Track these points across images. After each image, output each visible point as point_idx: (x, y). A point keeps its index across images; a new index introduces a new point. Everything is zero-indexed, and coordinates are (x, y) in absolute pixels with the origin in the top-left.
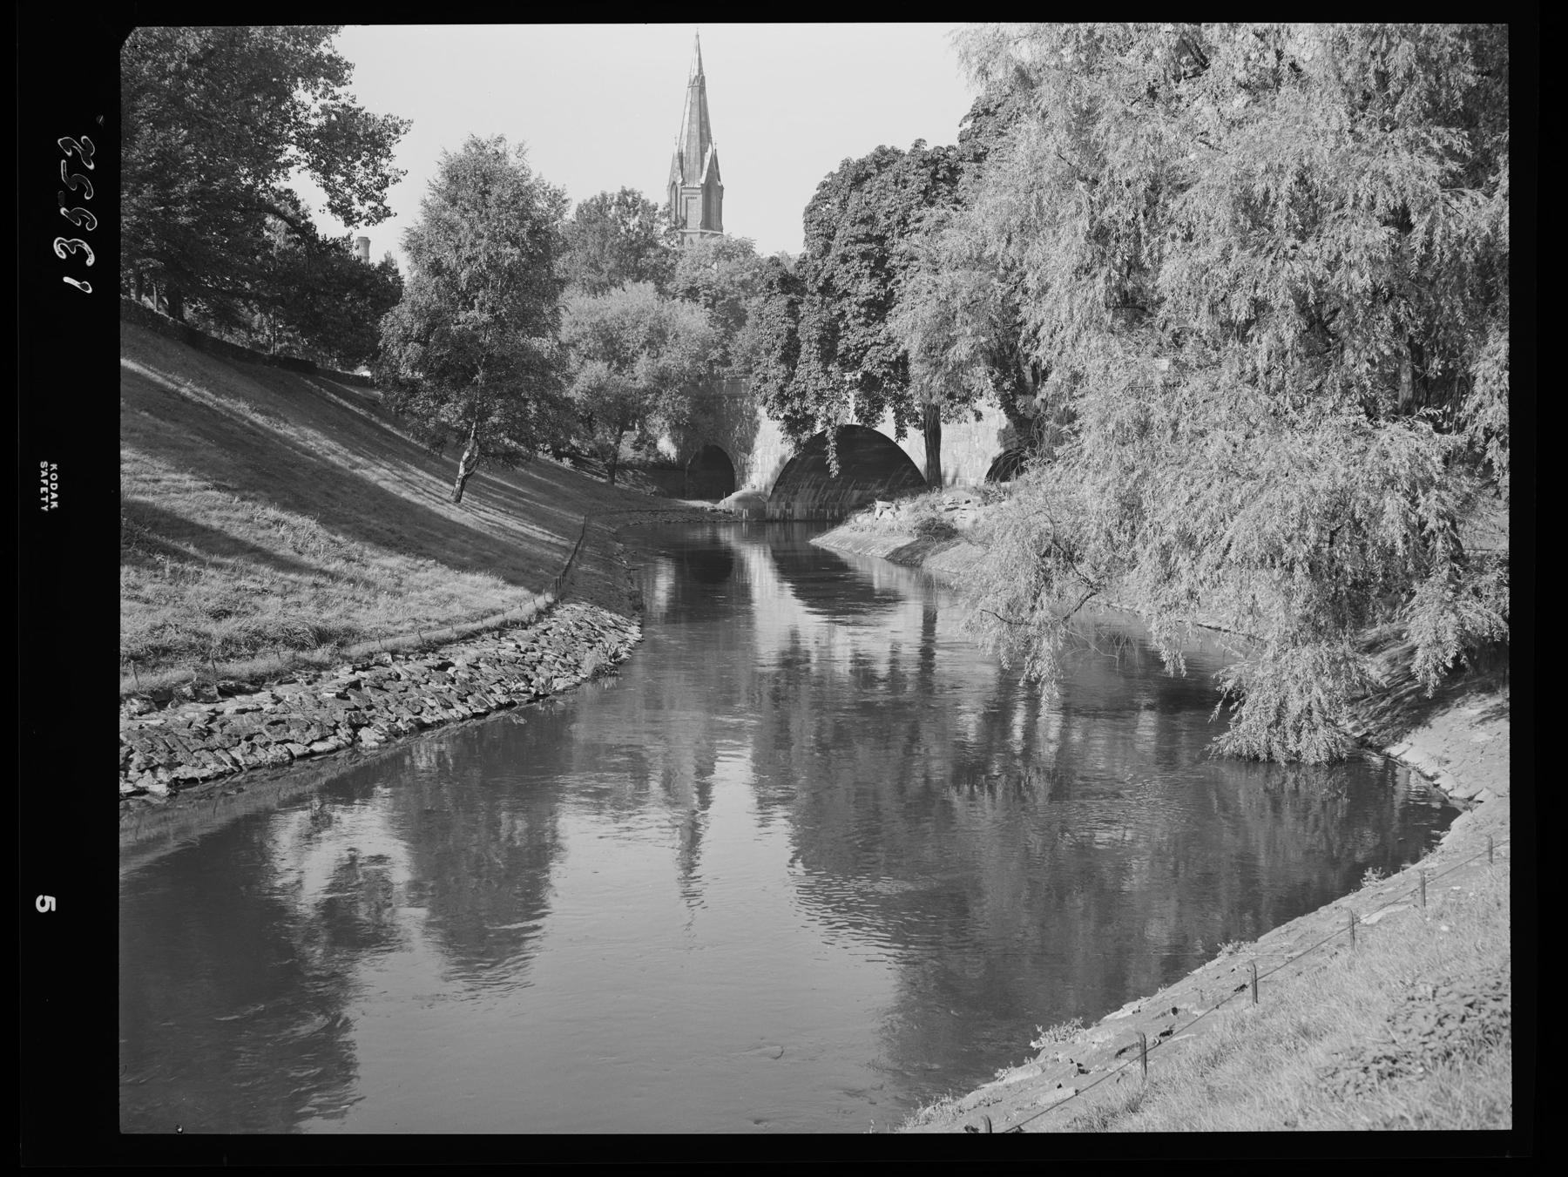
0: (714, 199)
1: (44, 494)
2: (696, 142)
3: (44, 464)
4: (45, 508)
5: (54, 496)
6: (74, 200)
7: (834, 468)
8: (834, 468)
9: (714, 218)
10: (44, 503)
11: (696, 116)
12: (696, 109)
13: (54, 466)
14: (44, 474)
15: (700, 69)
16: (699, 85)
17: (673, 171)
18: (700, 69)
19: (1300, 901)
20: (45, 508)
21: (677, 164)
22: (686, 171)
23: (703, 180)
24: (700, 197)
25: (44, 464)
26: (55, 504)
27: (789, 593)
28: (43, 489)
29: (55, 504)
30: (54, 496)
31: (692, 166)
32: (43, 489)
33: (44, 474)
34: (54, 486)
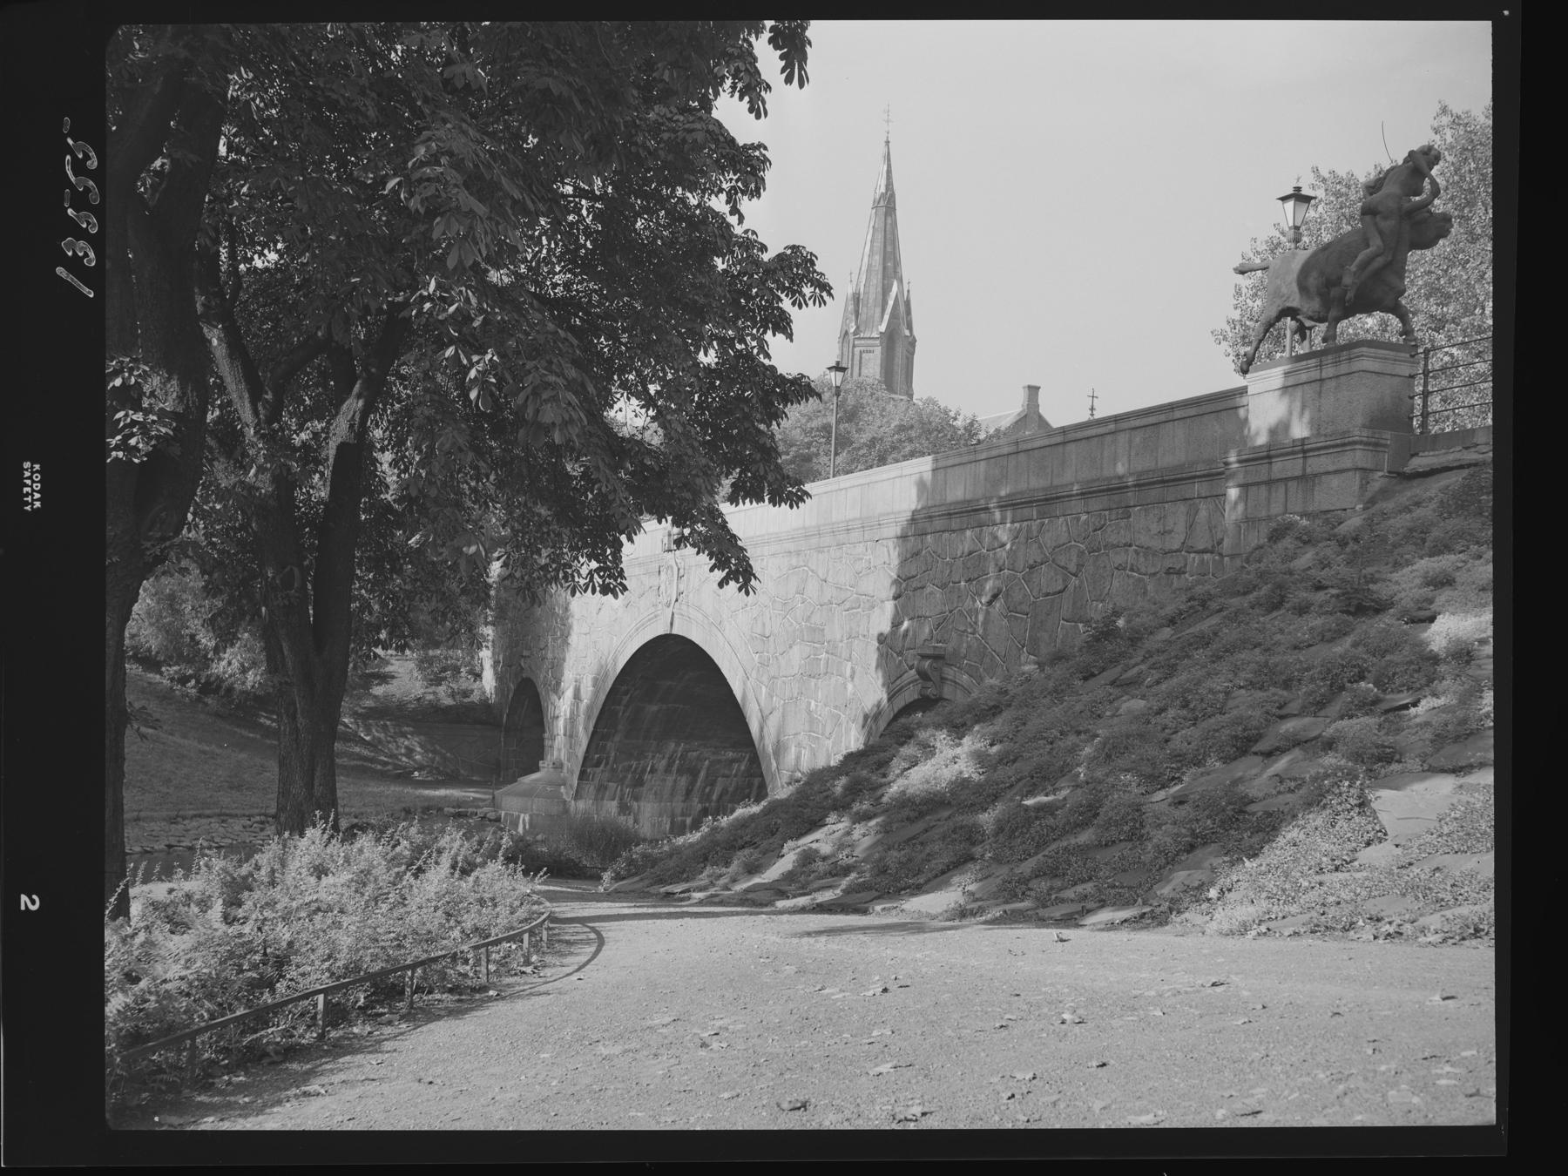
0: (900, 351)
1: (27, 494)
2: (876, 280)
3: (27, 465)
4: (28, 508)
5: (37, 496)
6: (81, 202)
7: (1029, 802)
8: (1029, 802)
9: (899, 378)
10: (27, 503)
11: (879, 244)
12: (880, 236)
13: (37, 467)
14: (27, 474)
15: (889, 185)
16: (887, 205)
17: (845, 318)
18: (889, 185)
19: (755, 760)
20: (28, 508)
21: (851, 307)
22: (863, 317)
23: (883, 328)
24: (878, 350)
25: (27, 465)
26: (38, 504)
27: (880, 681)
28: (26, 490)
29: (38, 504)
30: (37, 496)
31: (870, 309)
32: (26, 490)
33: (27, 474)
34: (37, 486)
